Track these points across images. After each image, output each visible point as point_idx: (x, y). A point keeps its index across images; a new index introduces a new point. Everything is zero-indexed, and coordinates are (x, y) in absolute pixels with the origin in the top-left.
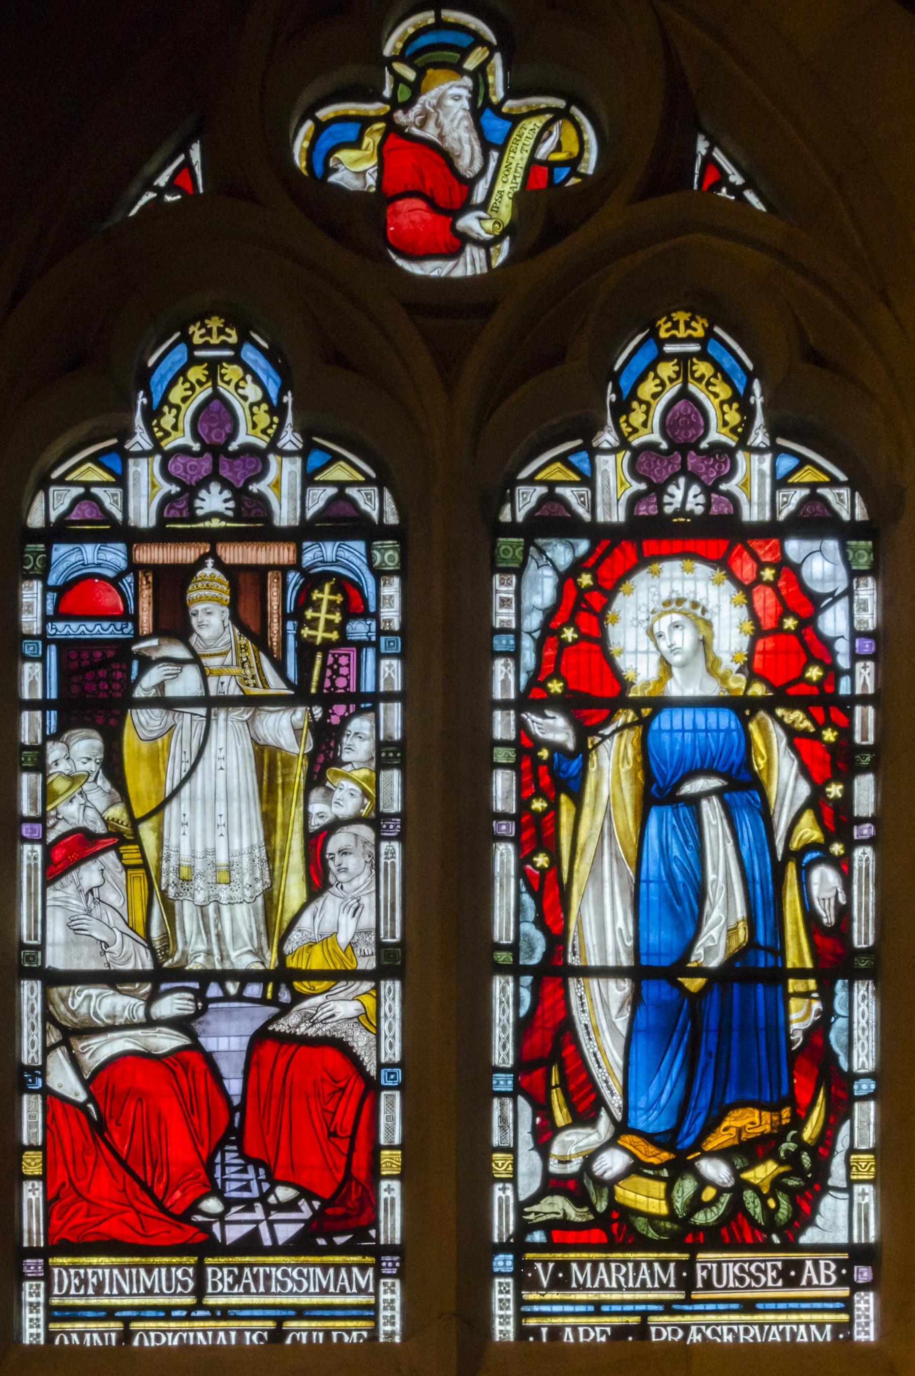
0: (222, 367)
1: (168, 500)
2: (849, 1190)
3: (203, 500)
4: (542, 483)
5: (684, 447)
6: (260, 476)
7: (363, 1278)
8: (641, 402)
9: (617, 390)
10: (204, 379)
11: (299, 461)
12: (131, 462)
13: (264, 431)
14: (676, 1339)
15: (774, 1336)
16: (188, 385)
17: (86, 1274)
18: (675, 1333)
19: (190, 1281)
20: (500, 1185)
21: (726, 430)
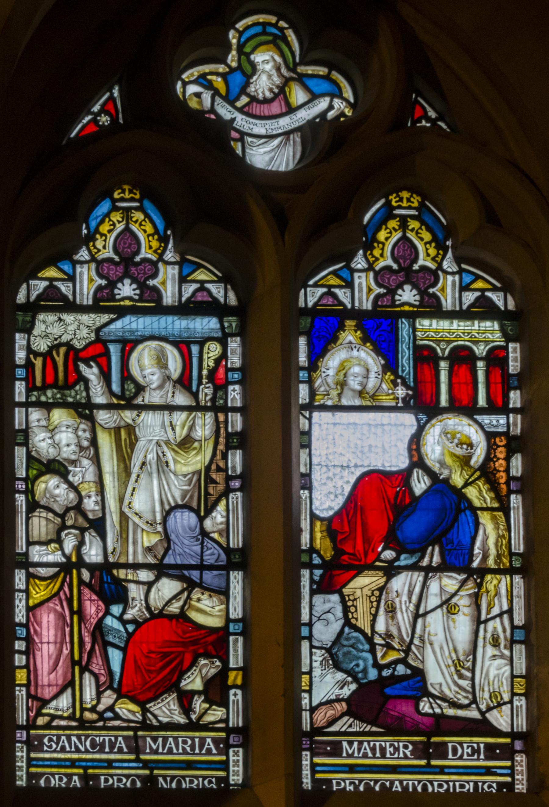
0: (132, 213)
1: (100, 288)
2: (511, 702)
3: (120, 289)
4: (323, 286)
5: (126, 262)
6: (155, 275)
7: (351, 748)
8: (102, 235)
9: (88, 228)
10: (397, 227)
11: (177, 267)
12: (78, 266)
13: (155, 251)
14: (441, 790)
15: (397, 787)
16: (388, 231)
17: (386, 745)
18: (61, 779)
19: (47, 743)
20: (517, 698)
21: (150, 251)
